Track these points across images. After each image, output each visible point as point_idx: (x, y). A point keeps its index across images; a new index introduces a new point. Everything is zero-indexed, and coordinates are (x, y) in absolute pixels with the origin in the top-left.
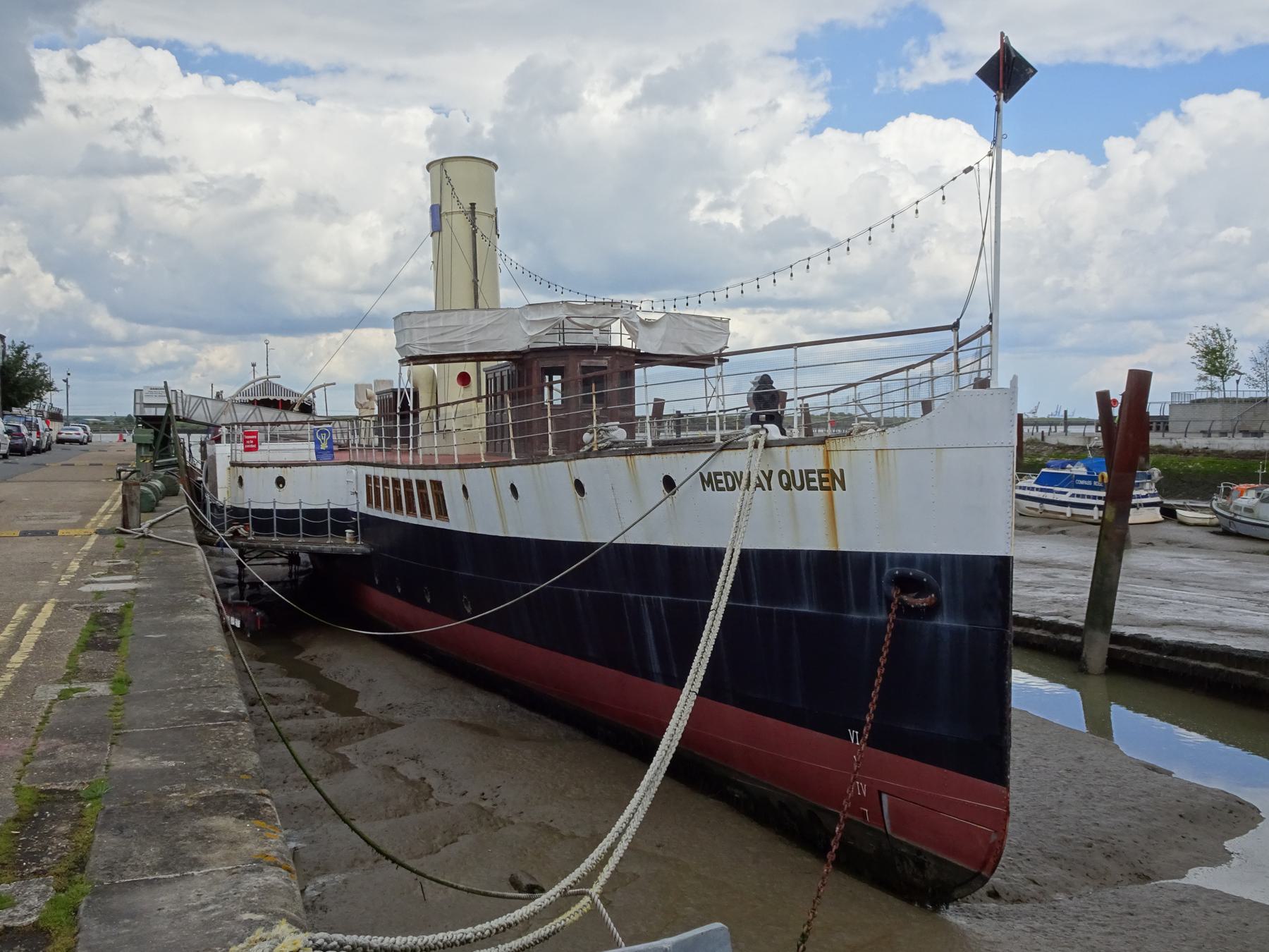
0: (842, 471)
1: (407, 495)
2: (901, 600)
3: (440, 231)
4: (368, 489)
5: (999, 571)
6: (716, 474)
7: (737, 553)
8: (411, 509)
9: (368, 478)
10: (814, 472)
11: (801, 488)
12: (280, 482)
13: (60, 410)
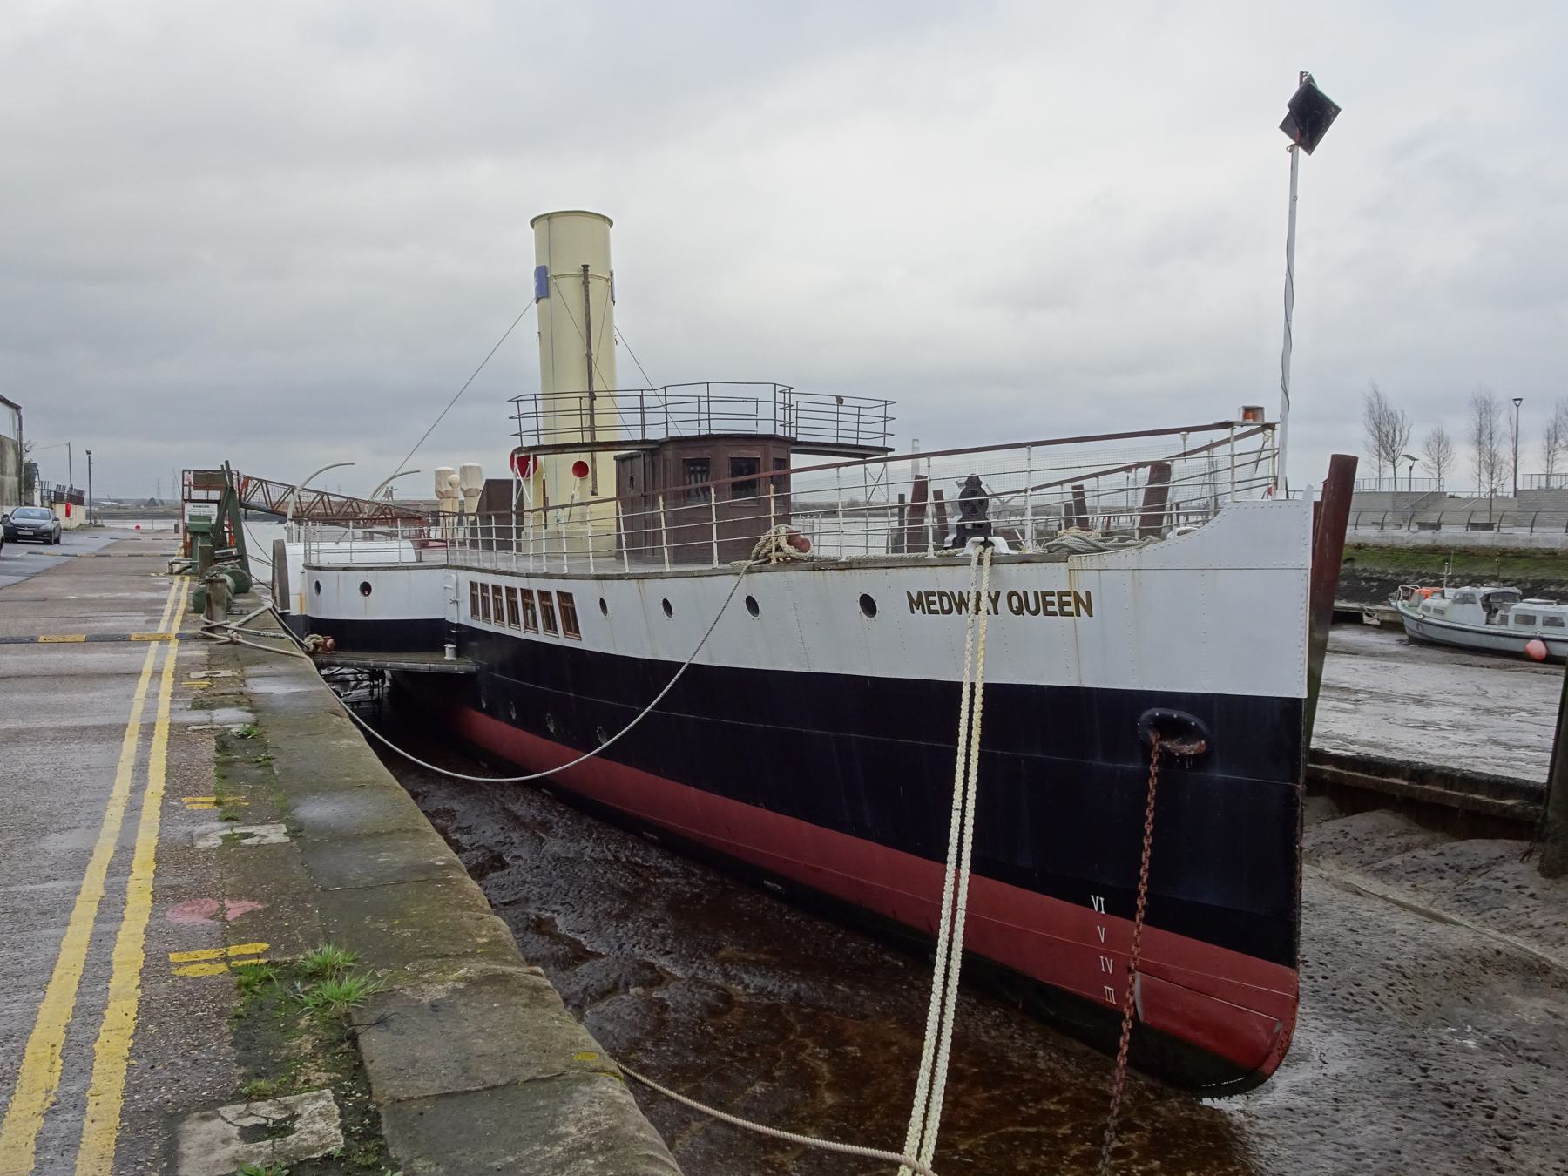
0: (1088, 594)
1: (518, 603)
2: (1161, 747)
3: (547, 296)
4: (473, 597)
5: (1291, 717)
6: (928, 594)
7: (979, 692)
8: (550, 625)
9: (473, 585)
10: (1052, 594)
11: (1036, 613)
12: (366, 588)
13: (81, 493)
